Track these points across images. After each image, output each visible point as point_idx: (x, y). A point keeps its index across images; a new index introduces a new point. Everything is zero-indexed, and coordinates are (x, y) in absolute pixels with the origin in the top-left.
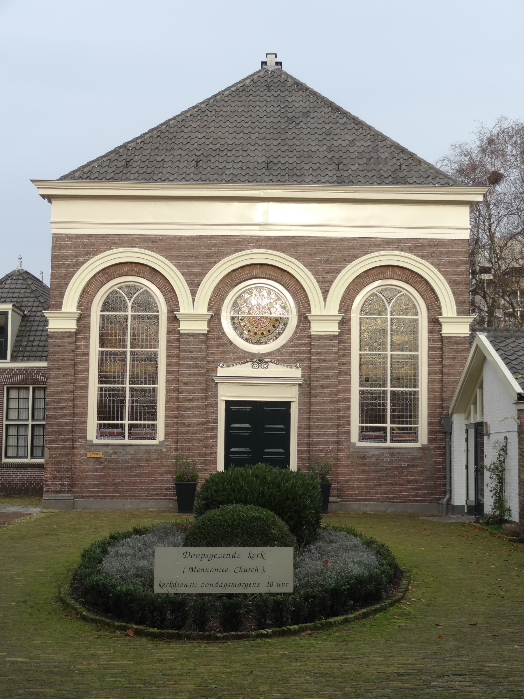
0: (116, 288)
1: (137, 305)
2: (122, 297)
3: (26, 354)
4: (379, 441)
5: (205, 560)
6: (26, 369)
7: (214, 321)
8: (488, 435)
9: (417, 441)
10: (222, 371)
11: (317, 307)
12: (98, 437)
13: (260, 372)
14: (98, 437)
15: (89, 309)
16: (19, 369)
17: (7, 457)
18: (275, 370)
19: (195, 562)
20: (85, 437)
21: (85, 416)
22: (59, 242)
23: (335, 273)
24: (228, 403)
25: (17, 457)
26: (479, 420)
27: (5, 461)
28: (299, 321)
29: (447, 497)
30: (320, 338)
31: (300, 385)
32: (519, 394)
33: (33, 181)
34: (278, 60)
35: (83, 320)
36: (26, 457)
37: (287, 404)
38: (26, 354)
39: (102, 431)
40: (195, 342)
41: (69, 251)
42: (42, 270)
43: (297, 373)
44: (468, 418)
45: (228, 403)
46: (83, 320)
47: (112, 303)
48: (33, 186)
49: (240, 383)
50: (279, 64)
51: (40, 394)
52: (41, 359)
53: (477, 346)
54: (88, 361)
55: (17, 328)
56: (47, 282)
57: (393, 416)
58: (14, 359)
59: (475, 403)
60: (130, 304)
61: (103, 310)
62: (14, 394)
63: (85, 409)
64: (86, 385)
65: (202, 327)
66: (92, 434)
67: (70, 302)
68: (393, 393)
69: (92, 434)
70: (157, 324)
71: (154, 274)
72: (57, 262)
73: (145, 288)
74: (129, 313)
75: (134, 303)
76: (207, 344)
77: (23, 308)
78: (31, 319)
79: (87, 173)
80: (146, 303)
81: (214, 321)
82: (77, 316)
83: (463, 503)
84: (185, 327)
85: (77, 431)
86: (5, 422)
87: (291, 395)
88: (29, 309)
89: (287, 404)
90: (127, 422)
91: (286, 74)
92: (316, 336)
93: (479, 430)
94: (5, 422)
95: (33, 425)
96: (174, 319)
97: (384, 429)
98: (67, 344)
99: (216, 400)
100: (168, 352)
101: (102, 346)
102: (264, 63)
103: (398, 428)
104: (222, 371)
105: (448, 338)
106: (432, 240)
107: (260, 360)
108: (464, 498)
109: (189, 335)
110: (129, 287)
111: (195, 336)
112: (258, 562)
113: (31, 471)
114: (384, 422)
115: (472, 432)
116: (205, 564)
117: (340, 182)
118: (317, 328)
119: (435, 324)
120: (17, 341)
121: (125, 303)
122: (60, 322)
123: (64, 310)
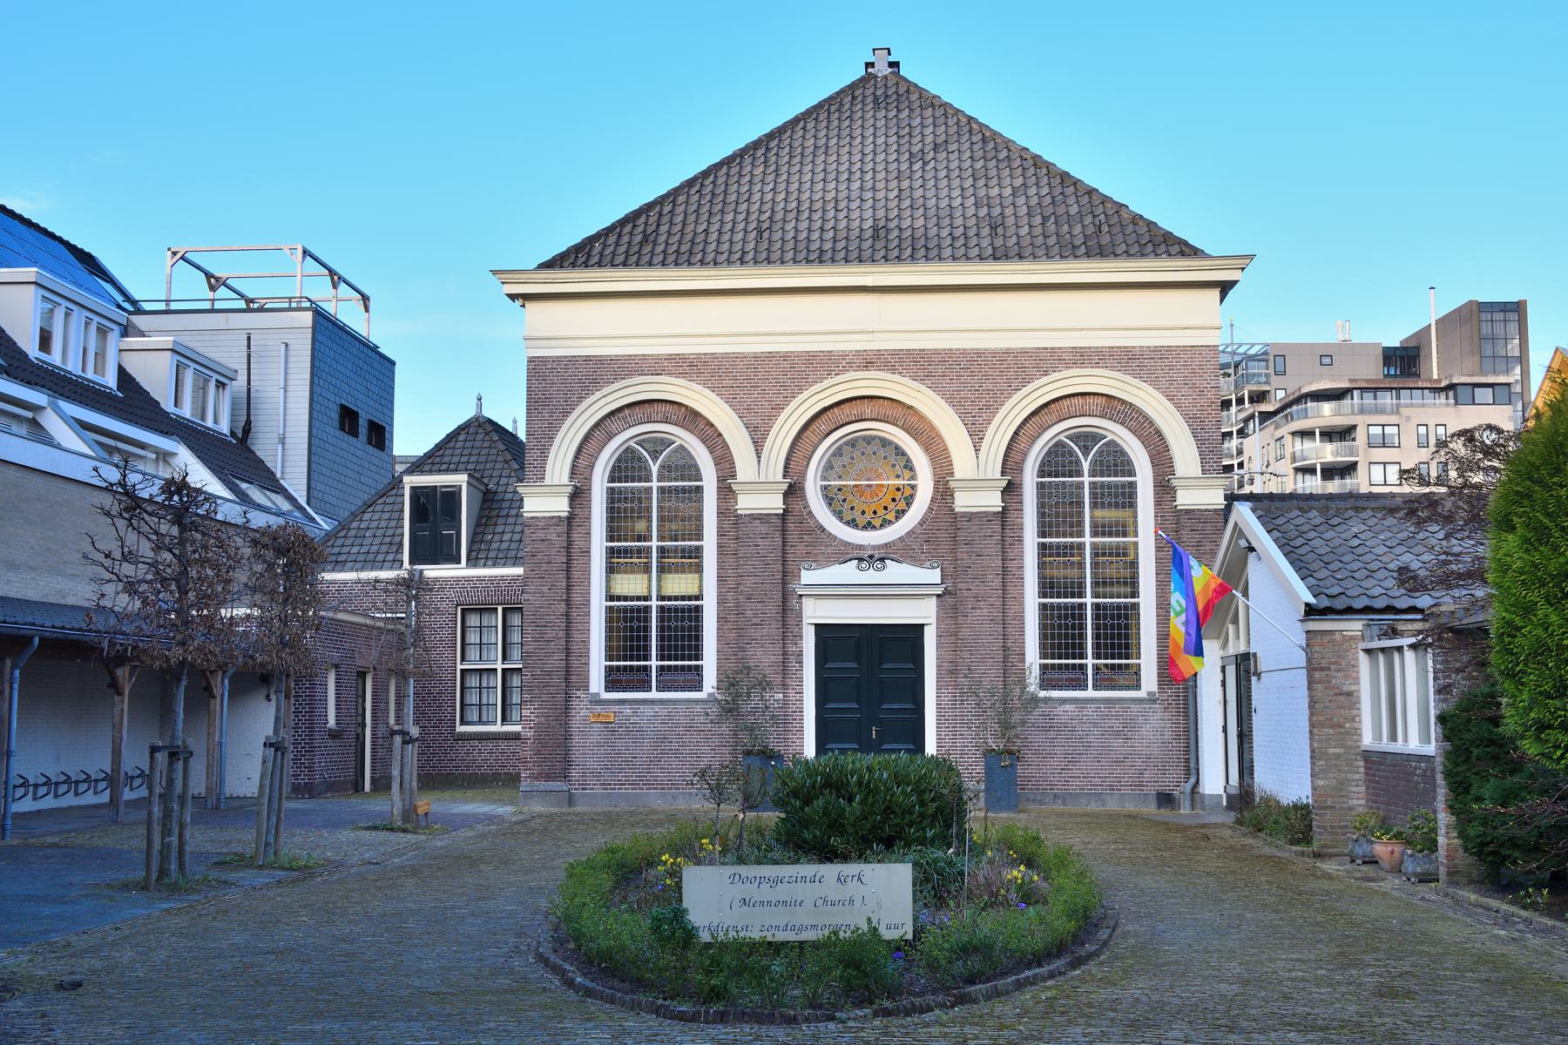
0: (1062, 437)
1: (667, 471)
2: (1071, 453)
3: (492, 554)
4: (1074, 688)
5: (765, 886)
6: (492, 579)
7: (794, 491)
8: (1258, 675)
9: (1138, 687)
10: (807, 577)
11: (745, 468)
12: (607, 689)
13: (871, 576)
14: (607, 689)
15: (589, 479)
16: (479, 579)
17: (463, 722)
18: (897, 572)
19: (750, 890)
20: (587, 688)
21: (586, 654)
22: (538, 370)
23: (992, 408)
24: (820, 628)
25: (480, 722)
26: (1242, 649)
27: (460, 729)
28: (936, 489)
29: (1193, 780)
30: (970, 517)
31: (938, 596)
32: (1307, 605)
33: (494, 272)
34: (891, 59)
35: (579, 496)
36: (495, 723)
37: (918, 629)
38: (492, 554)
39: (614, 680)
40: (764, 529)
41: (554, 384)
42: (511, 413)
43: (934, 576)
44: (1224, 646)
45: (820, 628)
46: (579, 496)
47: (1058, 462)
48: (495, 280)
49: (834, 596)
50: (894, 65)
51: (516, 620)
52: (516, 561)
53: (1236, 524)
54: (588, 563)
55: (475, 513)
56: (522, 435)
57: (1097, 646)
58: (473, 561)
59: (1235, 621)
60: (655, 469)
61: (612, 480)
62: (473, 620)
63: (586, 643)
64: (587, 603)
65: (775, 503)
66: (597, 682)
67: (558, 466)
68: (1097, 607)
69: (597, 682)
70: (700, 500)
71: (692, 419)
72: (535, 403)
73: (1110, 437)
74: (655, 484)
75: (662, 467)
76: (784, 531)
77: (486, 480)
78: (499, 497)
79: (578, 256)
80: (685, 467)
81: (794, 491)
82: (569, 489)
83: (1221, 791)
84: (747, 503)
85: (574, 679)
86: (459, 667)
87: (923, 612)
88: (495, 481)
89: (918, 629)
90: (654, 663)
91: (906, 80)
92: (964, 514)
93: (1245, 667)
94: (459, 667)
95: (504, 670)
96: (726, 491)
97: (1082, 667)
98: (554, 537)
99: (799, 624)
100: (720, 546)
101: (611, 539)
102: (869, 65)
103: (1106, 665)
104: (807, 577)
105: (1188, 512)
106: (1157, 349)
107: (875, 558)
108: (1222, 782)
109: (753, 517)
110: (654, 441)
111: (553, 521)
112: (853, 888)
113: (503, 744)
114: (1082, 656)
115: (1231, 671)
116: (766, 893)
117: (999, 255)
118: (964, 502)
119: (1164, 489)
120: (475, 534)
121: (1078, 462)
122: (543, 501)
123: (547, 481)
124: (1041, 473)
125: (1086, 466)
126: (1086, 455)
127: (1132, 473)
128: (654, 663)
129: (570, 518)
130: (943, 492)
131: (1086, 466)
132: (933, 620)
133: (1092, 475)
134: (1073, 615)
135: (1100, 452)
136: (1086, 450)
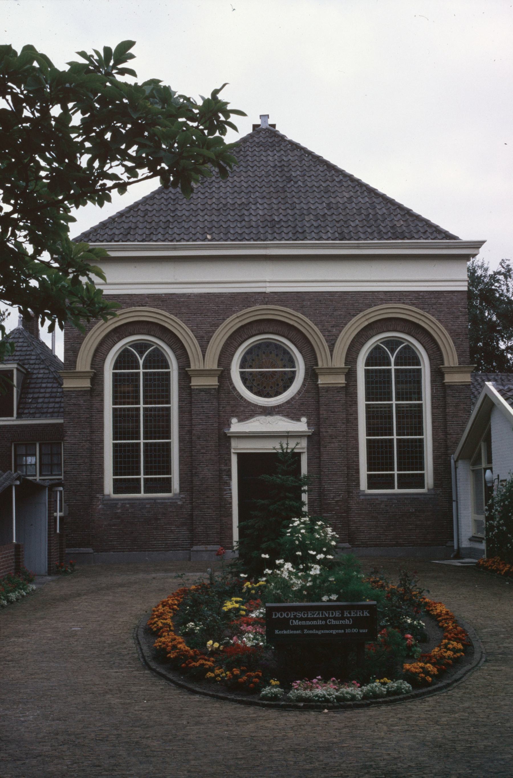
23: (340, 326)
24: (241, 456)
45: (241, 456)
53: (486, 395)
58: (20, 416)
66: (108, 488)
69: (108, 488)
81: (224, 375)
86: (38, 478)
92: (323, 388)
105: (450, 386)
107: (268, 411)
109: (201, 390)
121: (138, 362)
124: (367, 364)
125: (393, 360)
126: (392, 353)
127: (167, 367)
128: (142, 476)
129: (347, 386)
130: (312, 374)
131: (393, 360)
132: (305, 450)
133: (145, 367)
134: (386, 446)
135: (400, 351)
136: (141, 353)
